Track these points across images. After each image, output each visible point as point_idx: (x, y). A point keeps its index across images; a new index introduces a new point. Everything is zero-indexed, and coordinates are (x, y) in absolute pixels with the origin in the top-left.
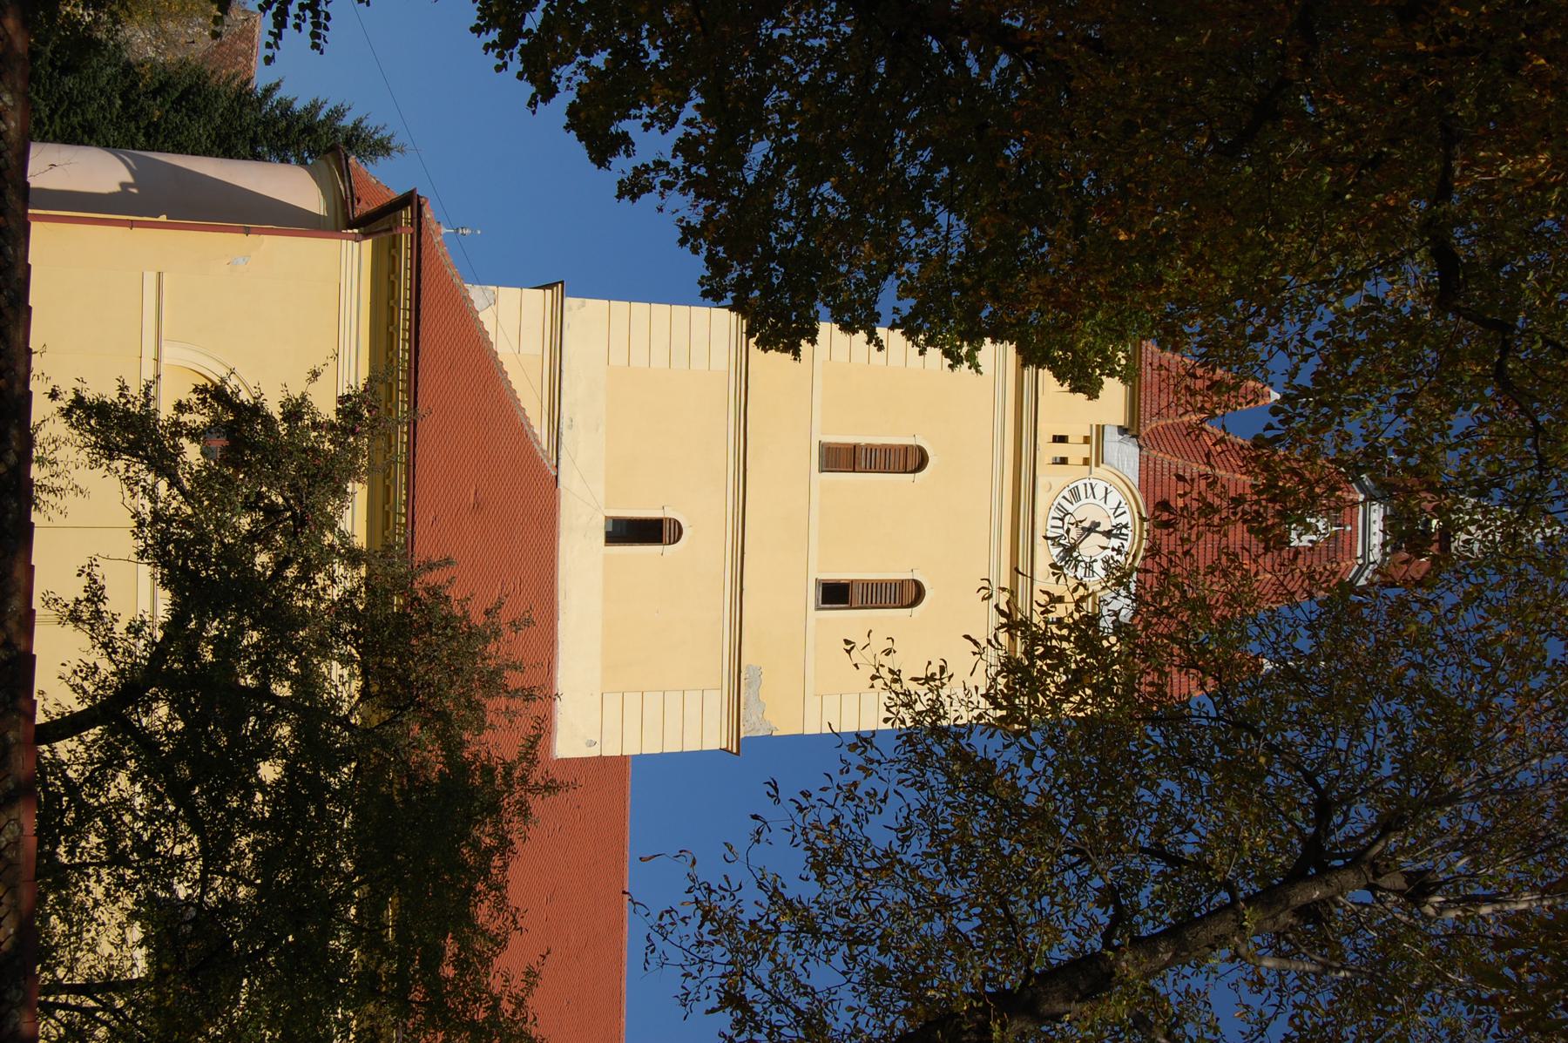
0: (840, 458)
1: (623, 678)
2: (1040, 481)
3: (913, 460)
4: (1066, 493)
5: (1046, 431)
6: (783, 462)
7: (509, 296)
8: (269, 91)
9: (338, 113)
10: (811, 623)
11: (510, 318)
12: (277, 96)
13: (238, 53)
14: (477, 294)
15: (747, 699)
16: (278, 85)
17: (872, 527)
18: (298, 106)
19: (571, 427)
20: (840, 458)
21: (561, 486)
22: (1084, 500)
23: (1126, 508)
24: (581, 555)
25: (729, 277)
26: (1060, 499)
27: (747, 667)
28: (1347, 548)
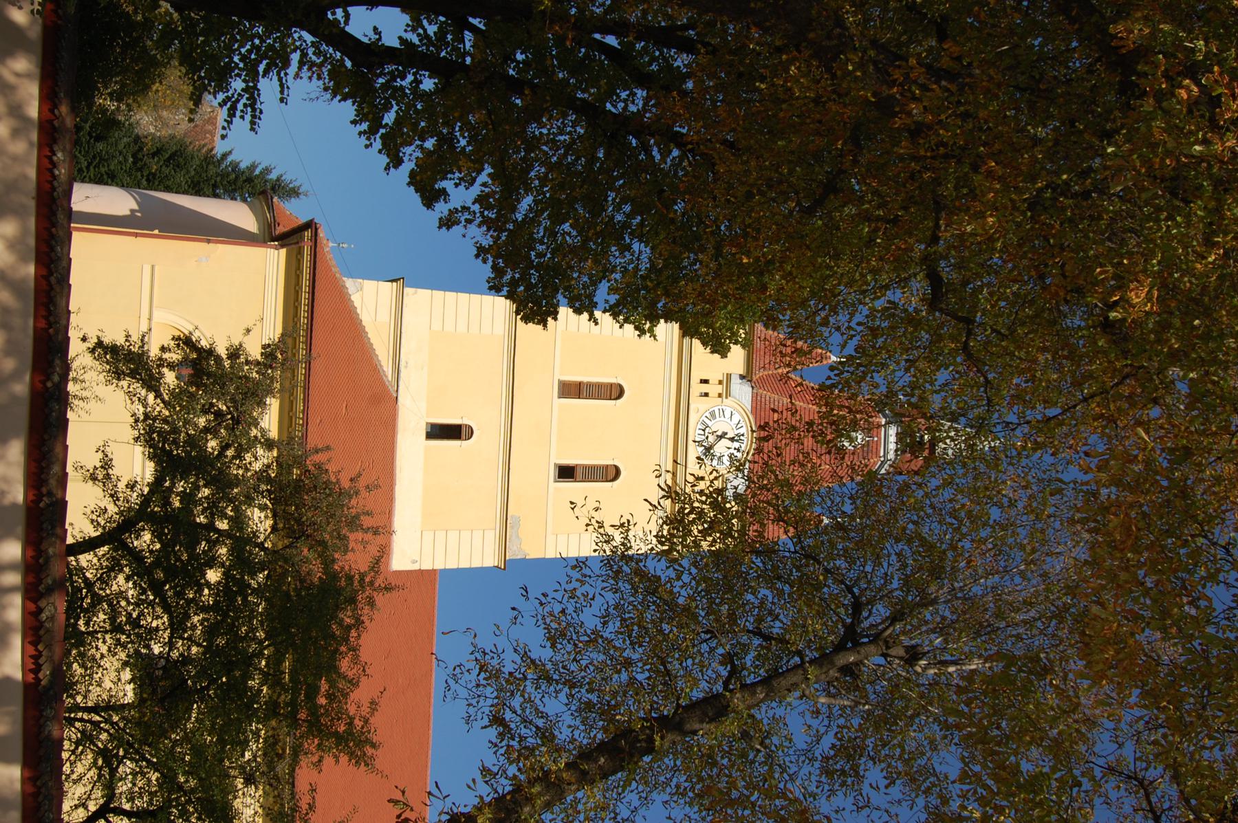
0: (571, 390)
1: (438, 521)
5: (696, 376)
7: (370, 285)
9: (267, 170)
11: (370, 299)
12: (230, 159)
14: (350, 284)
16: (231, 152)
18: (243, 166)
24: (412, 451)
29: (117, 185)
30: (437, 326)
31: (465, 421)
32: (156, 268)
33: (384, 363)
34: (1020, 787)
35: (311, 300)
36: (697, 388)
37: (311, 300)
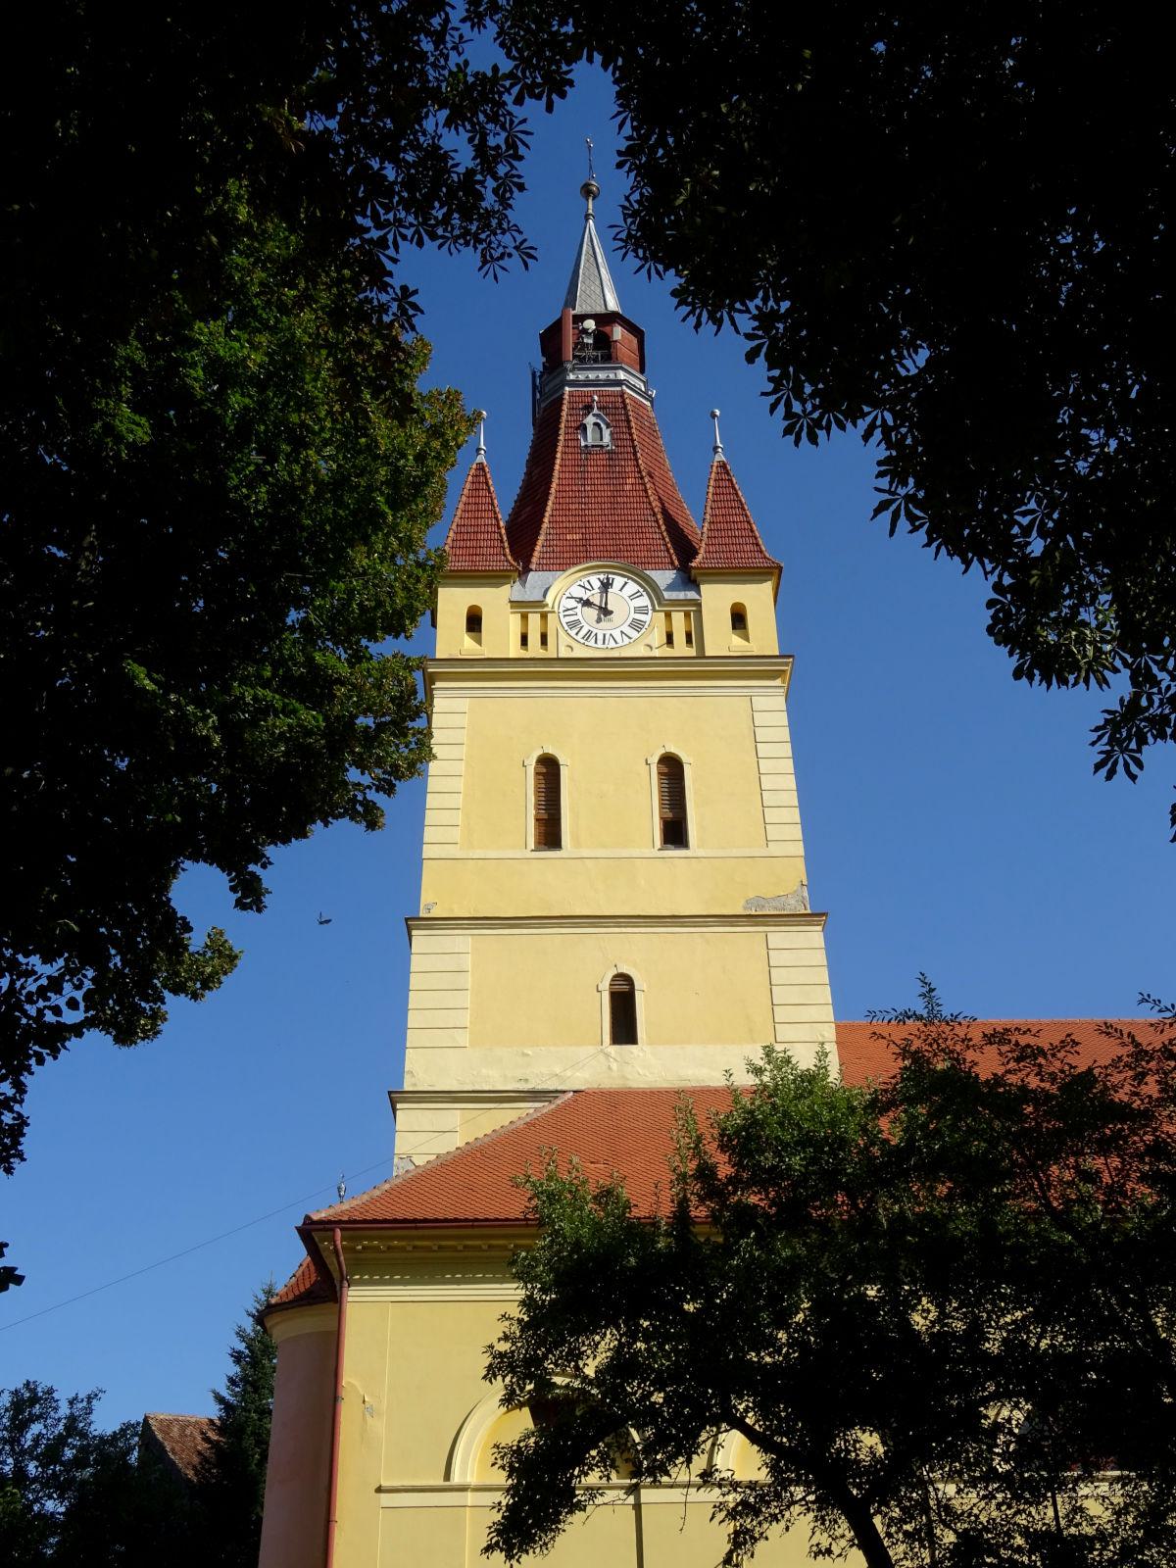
0: (550, 834)
1: (754, 1013)
2: (564, 653)
3: (549, 770)
4: (573, 633)
5: (514, 651)
6: (551, 884)
7: (403, 1144)
8: (220, 1399)
9: (241, 1334)
10: (701, 853)
11: (424, 1139)
12: (225, 1393)
13: (183, 1434)
14: (400, 1168)
15: (776, 908)
16: (214, 1392)
17: (611, 802)
18: (234, 1370)
19: (526, 1080)
20: (550, 834)
21: (583, 1088)
22: (579, 617)
23: (585, 580)
24: (647, 1066)
25: (140, 671)
26: (600, 644)
27: (745, 908)
28: (612, 399)
29: (330, 1301)
30: (463, 1038)
31: (605, 985)
32: (385, 1484)
33: (518, 1113)
34: (1077, 1167)
35: (419, 1241)
36: (535, 649)
37: (419, 1241)
